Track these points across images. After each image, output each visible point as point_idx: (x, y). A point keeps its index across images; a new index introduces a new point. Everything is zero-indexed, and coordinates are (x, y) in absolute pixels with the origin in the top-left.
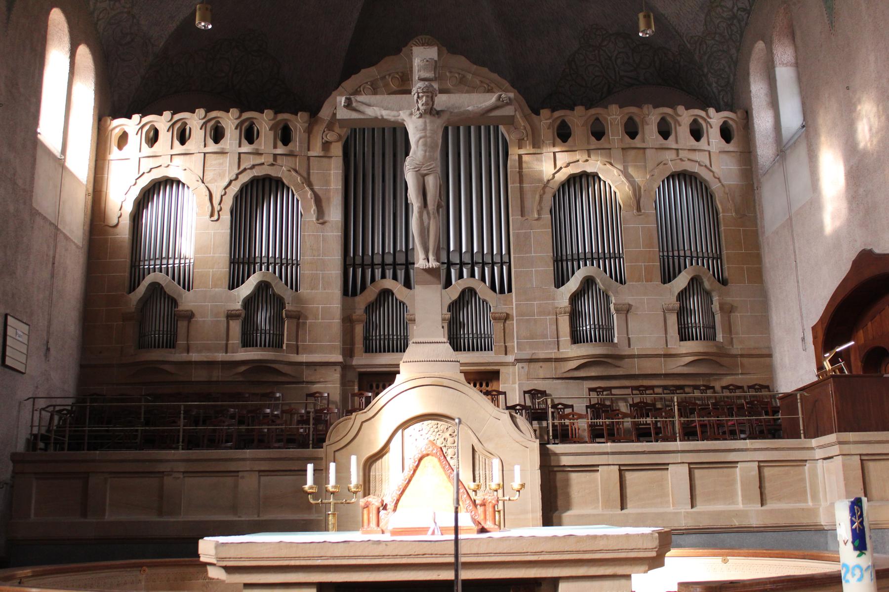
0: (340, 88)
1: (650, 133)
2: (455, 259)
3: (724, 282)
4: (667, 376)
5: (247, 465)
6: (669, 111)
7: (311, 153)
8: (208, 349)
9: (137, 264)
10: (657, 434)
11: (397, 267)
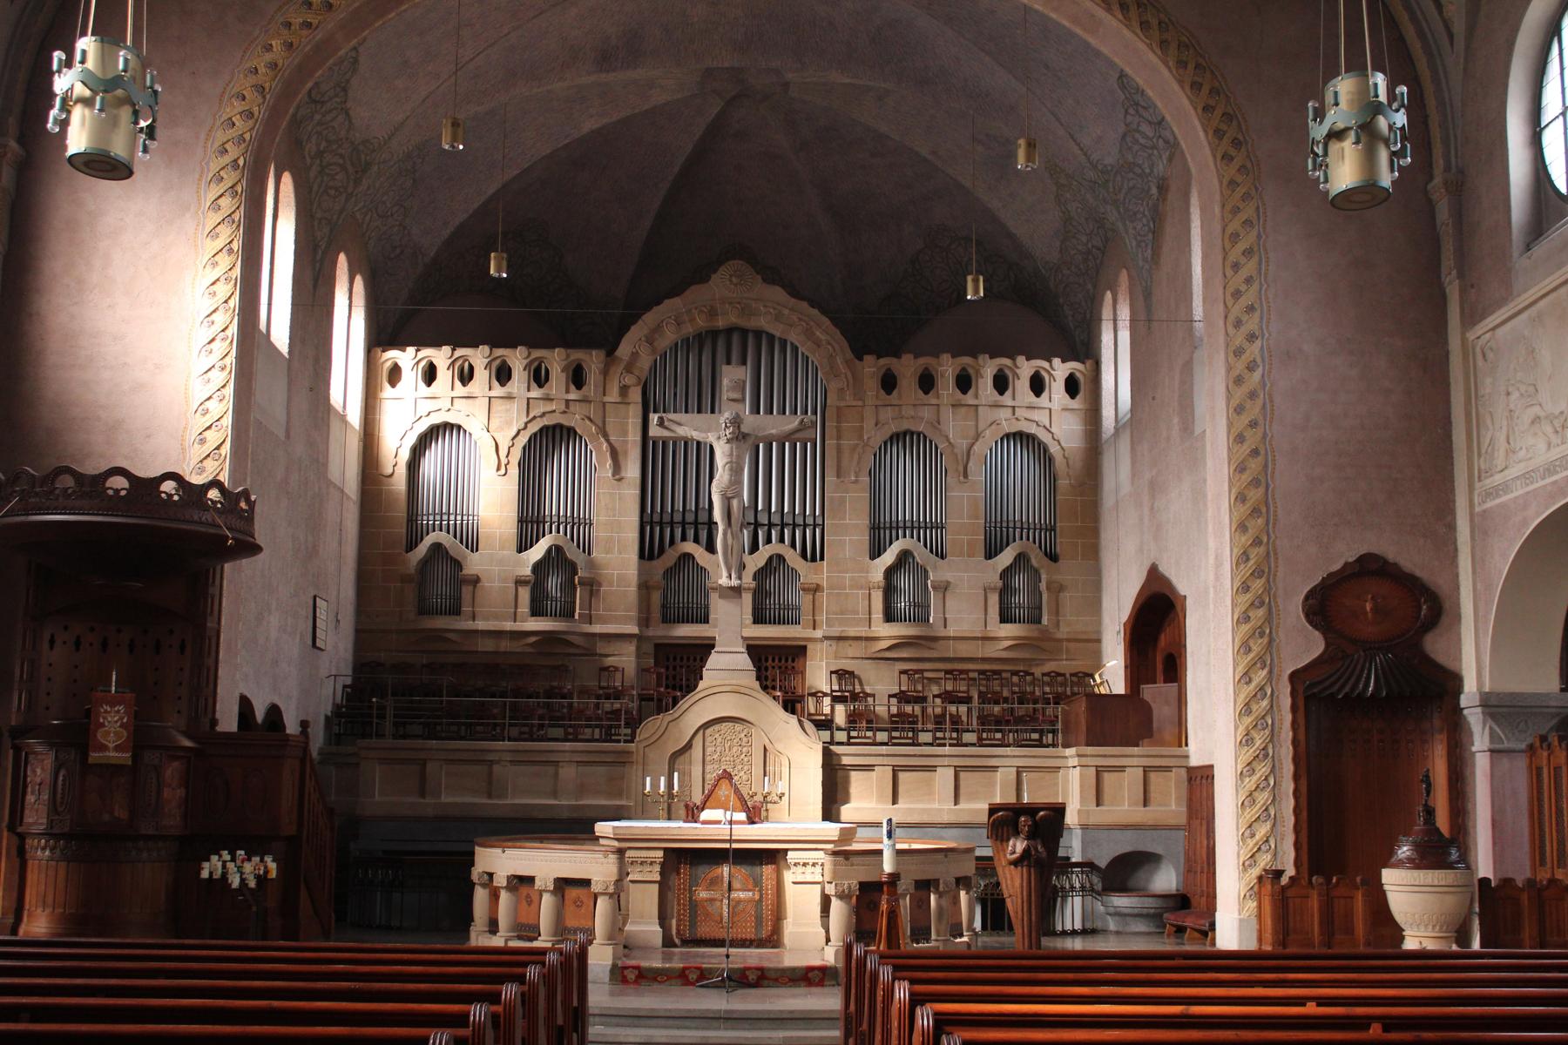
2: (763, 519)
4: (984, 660)
5: (567, 757)
6: (1008, 362)
7: (607, 399)
8: (497, 617)
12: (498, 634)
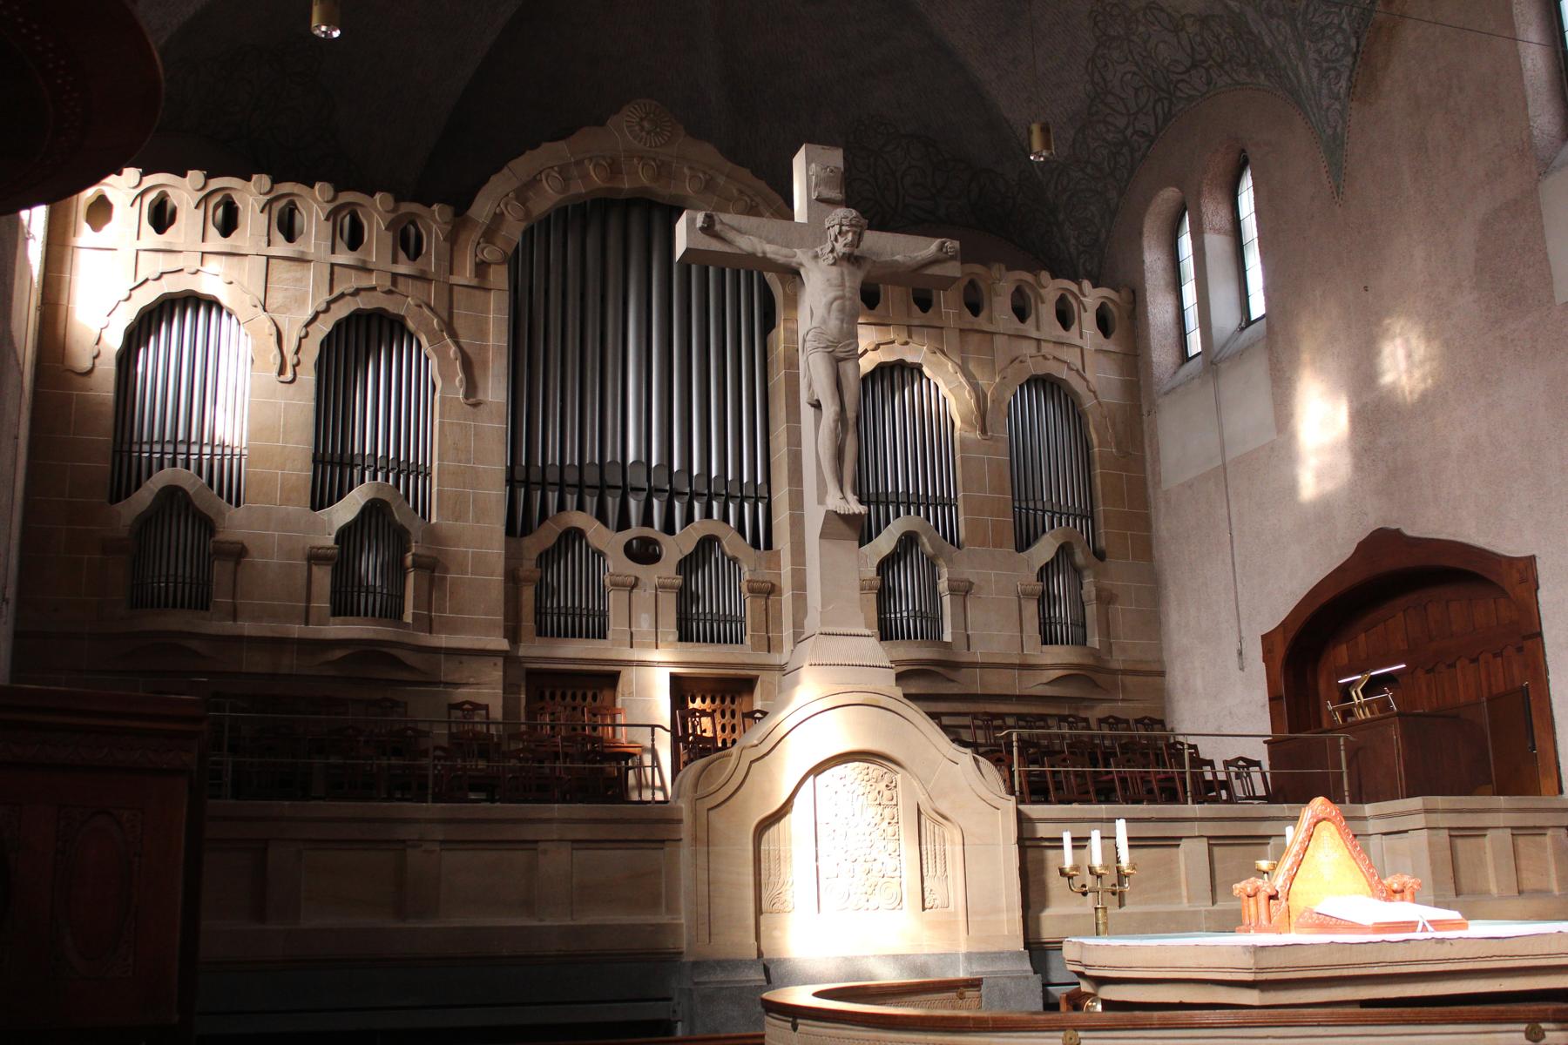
0: (505, 170)
1: (1001, 312)
3: (1100, 555)
7: (455, 279)
9: (126, 447)
10: (1125, 788)
11: (587, 491)
12: (278, 644)
